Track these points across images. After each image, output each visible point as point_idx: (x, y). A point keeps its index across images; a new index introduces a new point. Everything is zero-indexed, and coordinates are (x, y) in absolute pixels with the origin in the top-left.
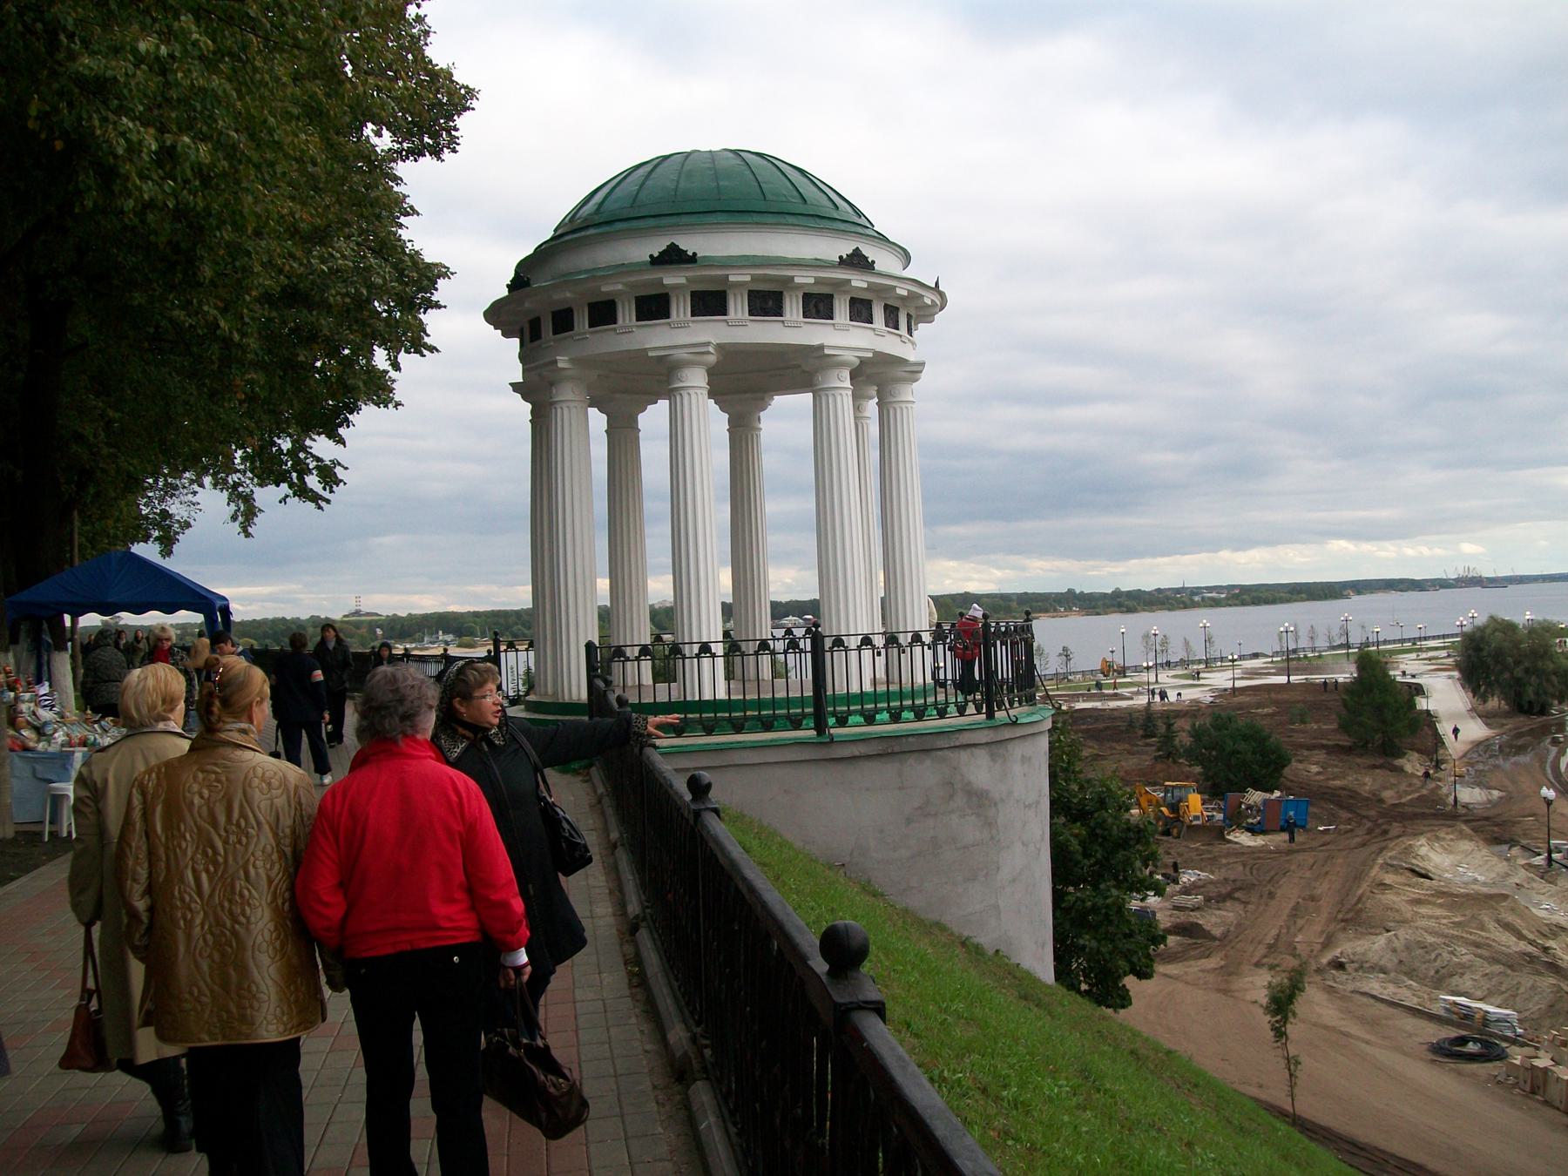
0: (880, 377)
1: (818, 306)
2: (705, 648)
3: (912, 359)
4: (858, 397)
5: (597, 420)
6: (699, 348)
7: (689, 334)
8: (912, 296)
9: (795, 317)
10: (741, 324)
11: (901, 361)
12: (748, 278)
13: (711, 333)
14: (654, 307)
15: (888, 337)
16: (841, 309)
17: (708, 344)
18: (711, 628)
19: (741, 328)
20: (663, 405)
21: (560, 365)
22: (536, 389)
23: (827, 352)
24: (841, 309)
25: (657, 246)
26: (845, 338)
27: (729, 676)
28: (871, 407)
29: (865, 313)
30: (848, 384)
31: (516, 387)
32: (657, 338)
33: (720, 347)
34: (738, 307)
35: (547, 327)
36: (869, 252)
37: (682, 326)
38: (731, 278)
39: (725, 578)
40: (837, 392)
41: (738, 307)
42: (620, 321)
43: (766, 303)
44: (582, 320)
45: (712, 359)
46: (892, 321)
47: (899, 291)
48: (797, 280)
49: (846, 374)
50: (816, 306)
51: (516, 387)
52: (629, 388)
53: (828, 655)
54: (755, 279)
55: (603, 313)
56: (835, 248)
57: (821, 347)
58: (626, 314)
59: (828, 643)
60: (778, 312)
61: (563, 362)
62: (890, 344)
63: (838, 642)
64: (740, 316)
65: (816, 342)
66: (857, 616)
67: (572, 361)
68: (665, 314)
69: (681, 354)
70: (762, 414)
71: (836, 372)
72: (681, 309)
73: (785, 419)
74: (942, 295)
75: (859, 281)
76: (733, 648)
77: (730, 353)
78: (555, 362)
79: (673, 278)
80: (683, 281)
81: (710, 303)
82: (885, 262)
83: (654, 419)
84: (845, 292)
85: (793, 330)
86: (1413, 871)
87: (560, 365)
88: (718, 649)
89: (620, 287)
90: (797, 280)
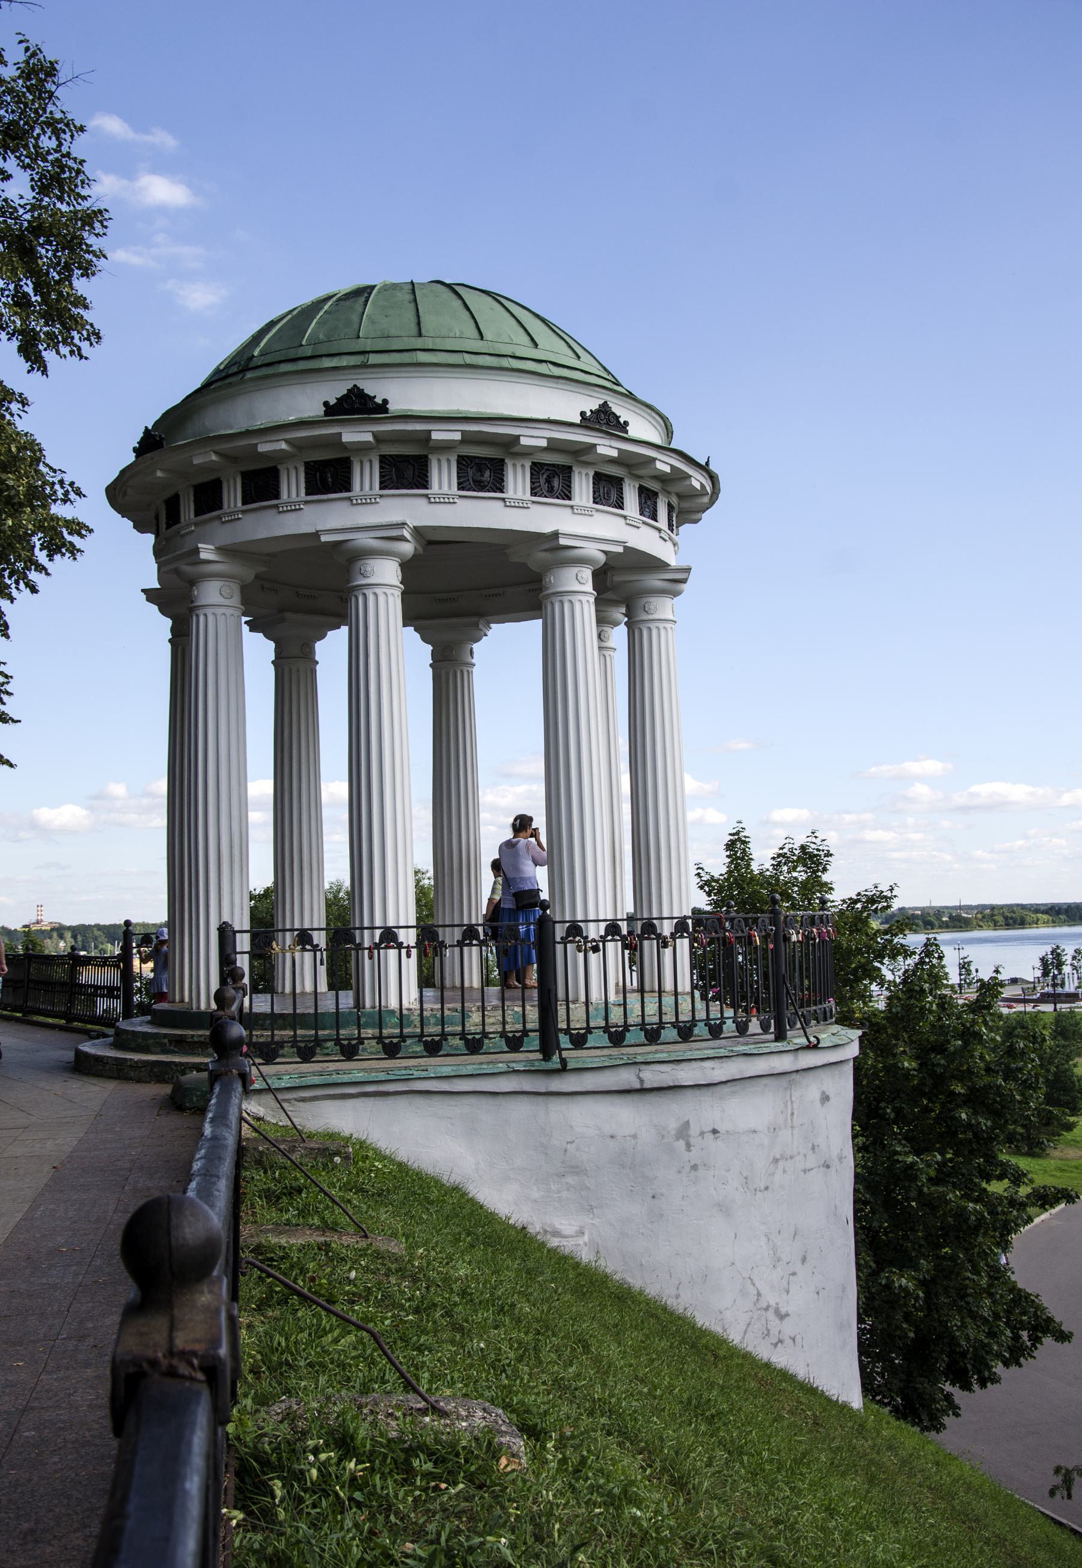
0: (626, 586)
1: (551, 479)
2: (389, 937)
3: (673, 562)
4: (602, 620)
5: (258, 653)
6: (391, 532)
7: (378, 518)
8: (677, 476)
9: (519, 495)
10: (447, 501)
11: (655, 565)
12: (457, 436)
13: (410, 511)
14: (330, 476)
15: (644, 528)
16: (582, 487)
17: (403, 524)
18: (399, 909)
19: (450, 508)
20: (344, 630)
21: (204, 556)
22: (175, 598)
23: (563, 541)
24: (582, 487)
25: (334, 390)
26: (589, 527)
27: (425, 981)
28: (618, 636)
29: (614, 496)
30: (589, 587)
31: (150, 595)
32: (330, 519)
33: (418, 531)
34: (443, 477)
35: (187, 511)
36: (622, 411)
37: (368, 501)
38: (435, 436)
39: (423, 856)
40: (575, 598)
41: (443, 477)
42: (284, 495)
43: (482, 471)
44: (233, 496)
45: (408, 548)
46: (648, 500)
47: (659, 465)
48: (524, 441)
49: (587, 574)
50: (548, 481)
51: (150, 595)
52: (302, 598)
53: (559, 948)
54: (468, 439)
55: (262, 486)
56: (570, 405)
57: (555, 535)
58: (292, 486)
59: (560, 932)
60: (498, 485)
61: (207, 552)
62: (646, 539)
63: (575, 930)
64: (445, 489)
65: (547, 529)
66: (603, 894)
67: (220, 550)
68: (346, 485)
69: (365, 540)
70: (476, 647)
71: (574, 570)
72: (366, 477)
73: (505, 656)
74: (713, 478)
75: (607, 448)
76: (429, 938)
77: (435, 545)
78: (197, 551)
79: (355, 434)
80: (369, 437)
81: (406, 470)
82: (641, 428)
83: (331, 650)
84: (587, 464)
85: (514, 511)
86: (749, 1324)
87: (204, 556)
88: (408, 937)
89: (284, 446)
90: (524, 441)
